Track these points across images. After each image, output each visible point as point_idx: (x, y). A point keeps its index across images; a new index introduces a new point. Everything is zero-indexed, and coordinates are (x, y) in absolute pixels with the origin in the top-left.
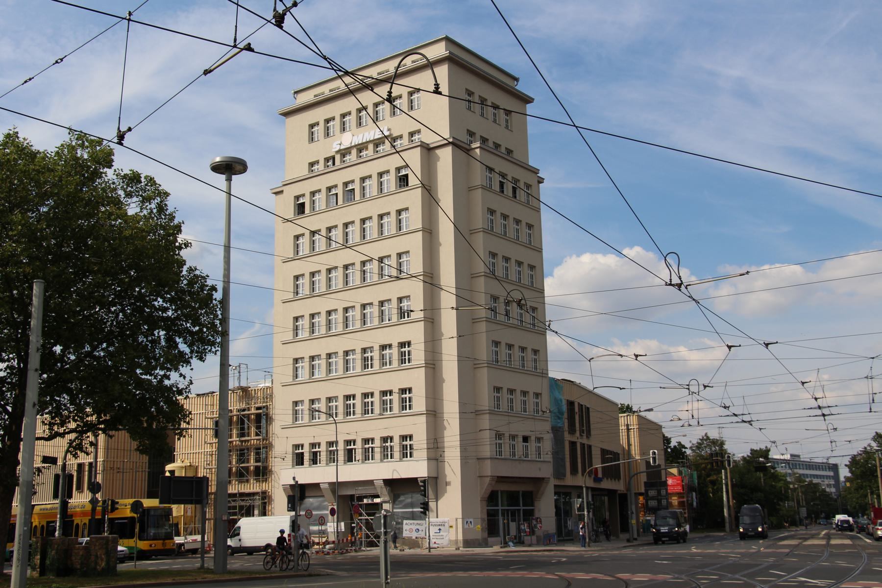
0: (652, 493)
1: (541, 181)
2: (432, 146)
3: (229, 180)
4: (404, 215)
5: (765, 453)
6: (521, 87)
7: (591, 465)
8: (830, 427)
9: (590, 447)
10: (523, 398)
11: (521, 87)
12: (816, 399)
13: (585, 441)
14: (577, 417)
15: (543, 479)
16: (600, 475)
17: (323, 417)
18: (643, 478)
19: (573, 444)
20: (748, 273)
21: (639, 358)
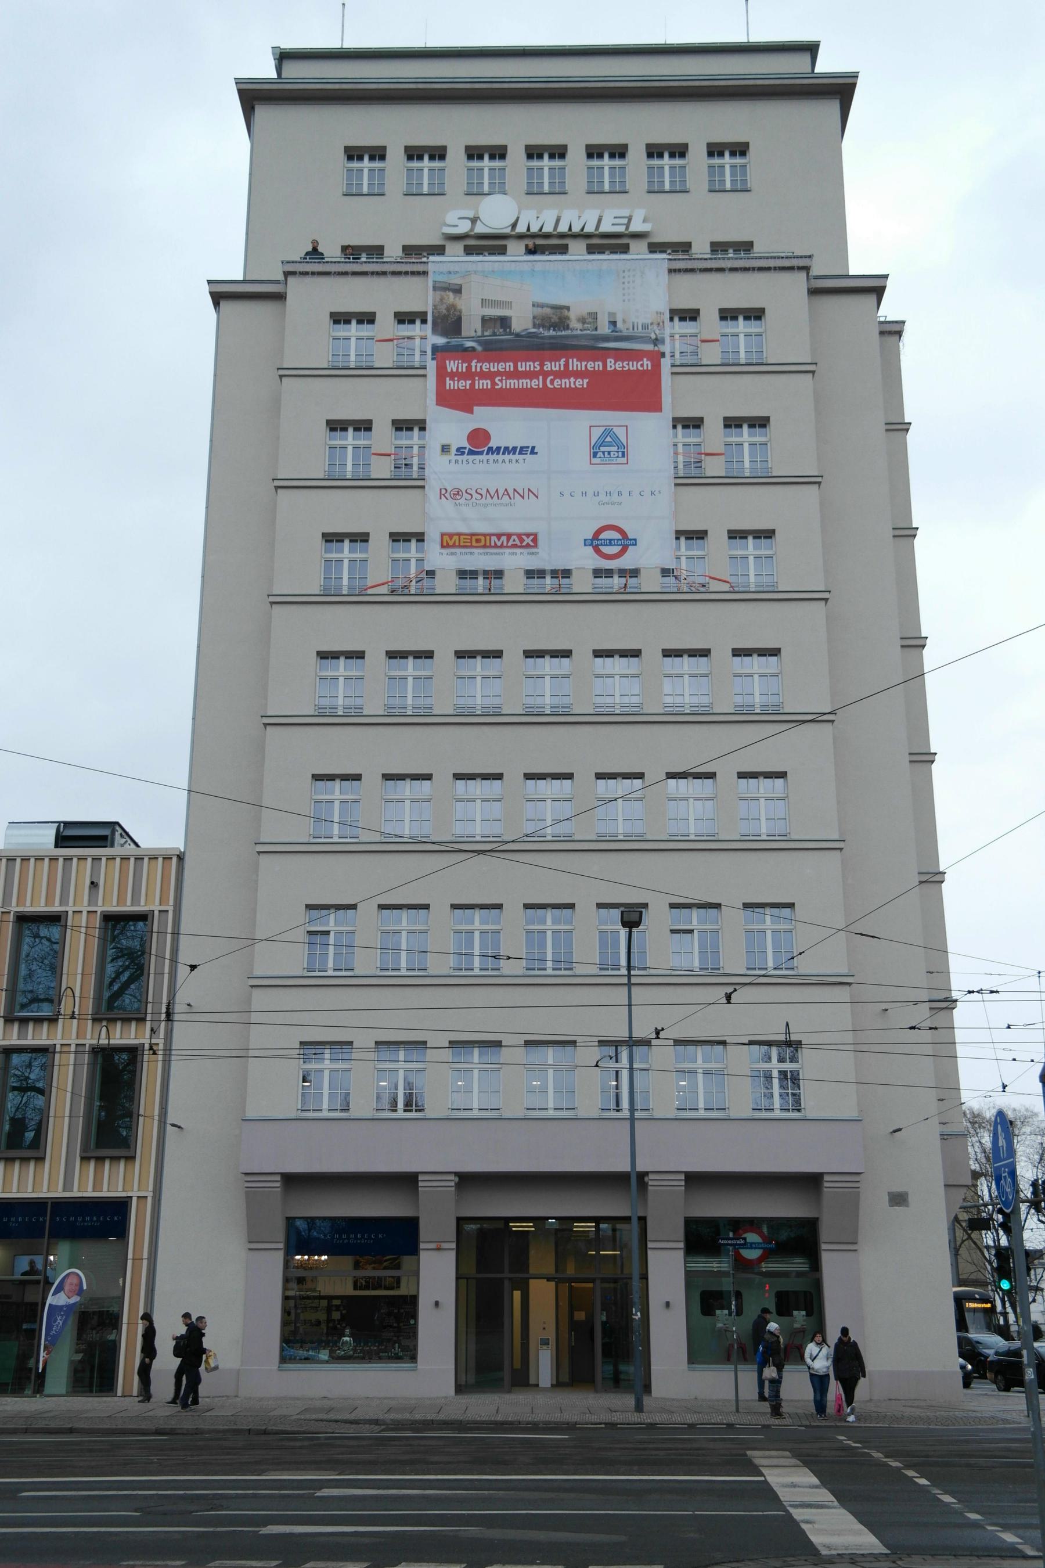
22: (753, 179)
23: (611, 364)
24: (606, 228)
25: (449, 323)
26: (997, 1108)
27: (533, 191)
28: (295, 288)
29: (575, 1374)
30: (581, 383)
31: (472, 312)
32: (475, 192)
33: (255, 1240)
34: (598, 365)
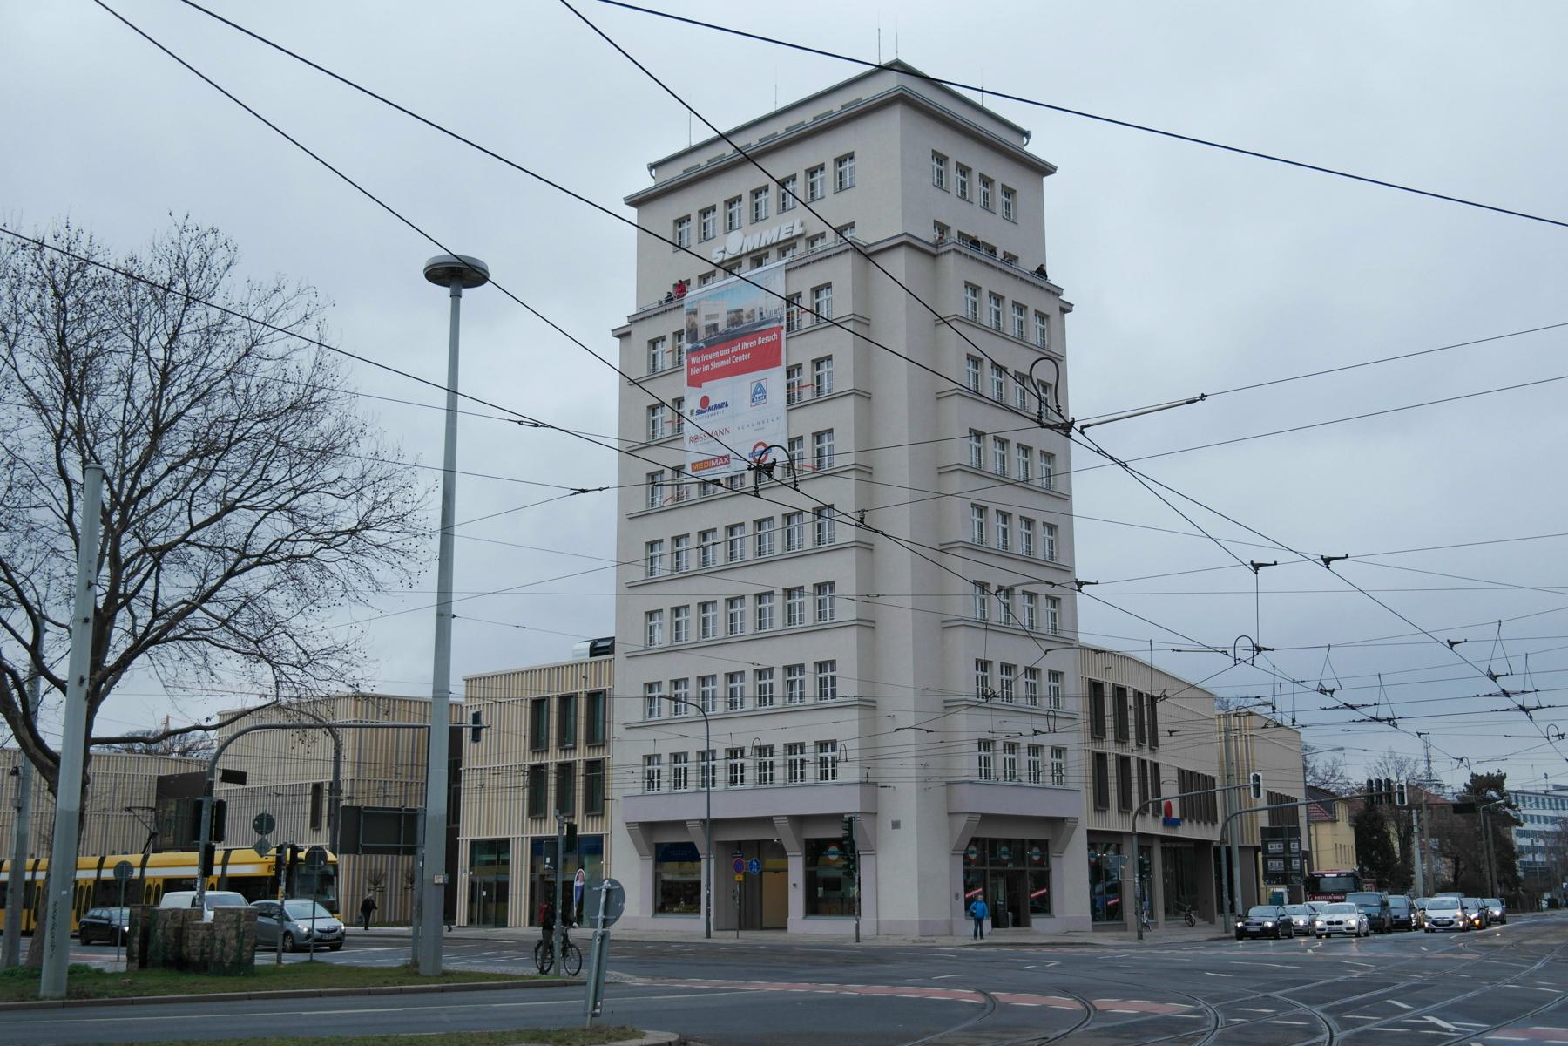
0: (1275, 847)
1: (1066, 308)
2: (871, 250)
3: (456, 296)
4: (825, 368)
5: (1496, 782)
6: (1034, 148)
7: (1157, 792)
8: (1553, 731)
9: (1156, 766)
10: (1053, 684)
11: (1033, 148)
12: (1494, 677)
13: (1146, 756)
14: (1131, 715)
15: (1063, 819)
16: (1176, 814)
17: (692, 711)
18: (1263, 820)
19: (1123, 762)
20: (1203, 397)
21: (1084, 588)
23: (761, 340)
24: (783, 237)
25: (693, 334)
28: (635, 330)
29: (813, 907)
30: (747, 356)
31: (702, 322)
34: (752, 344)
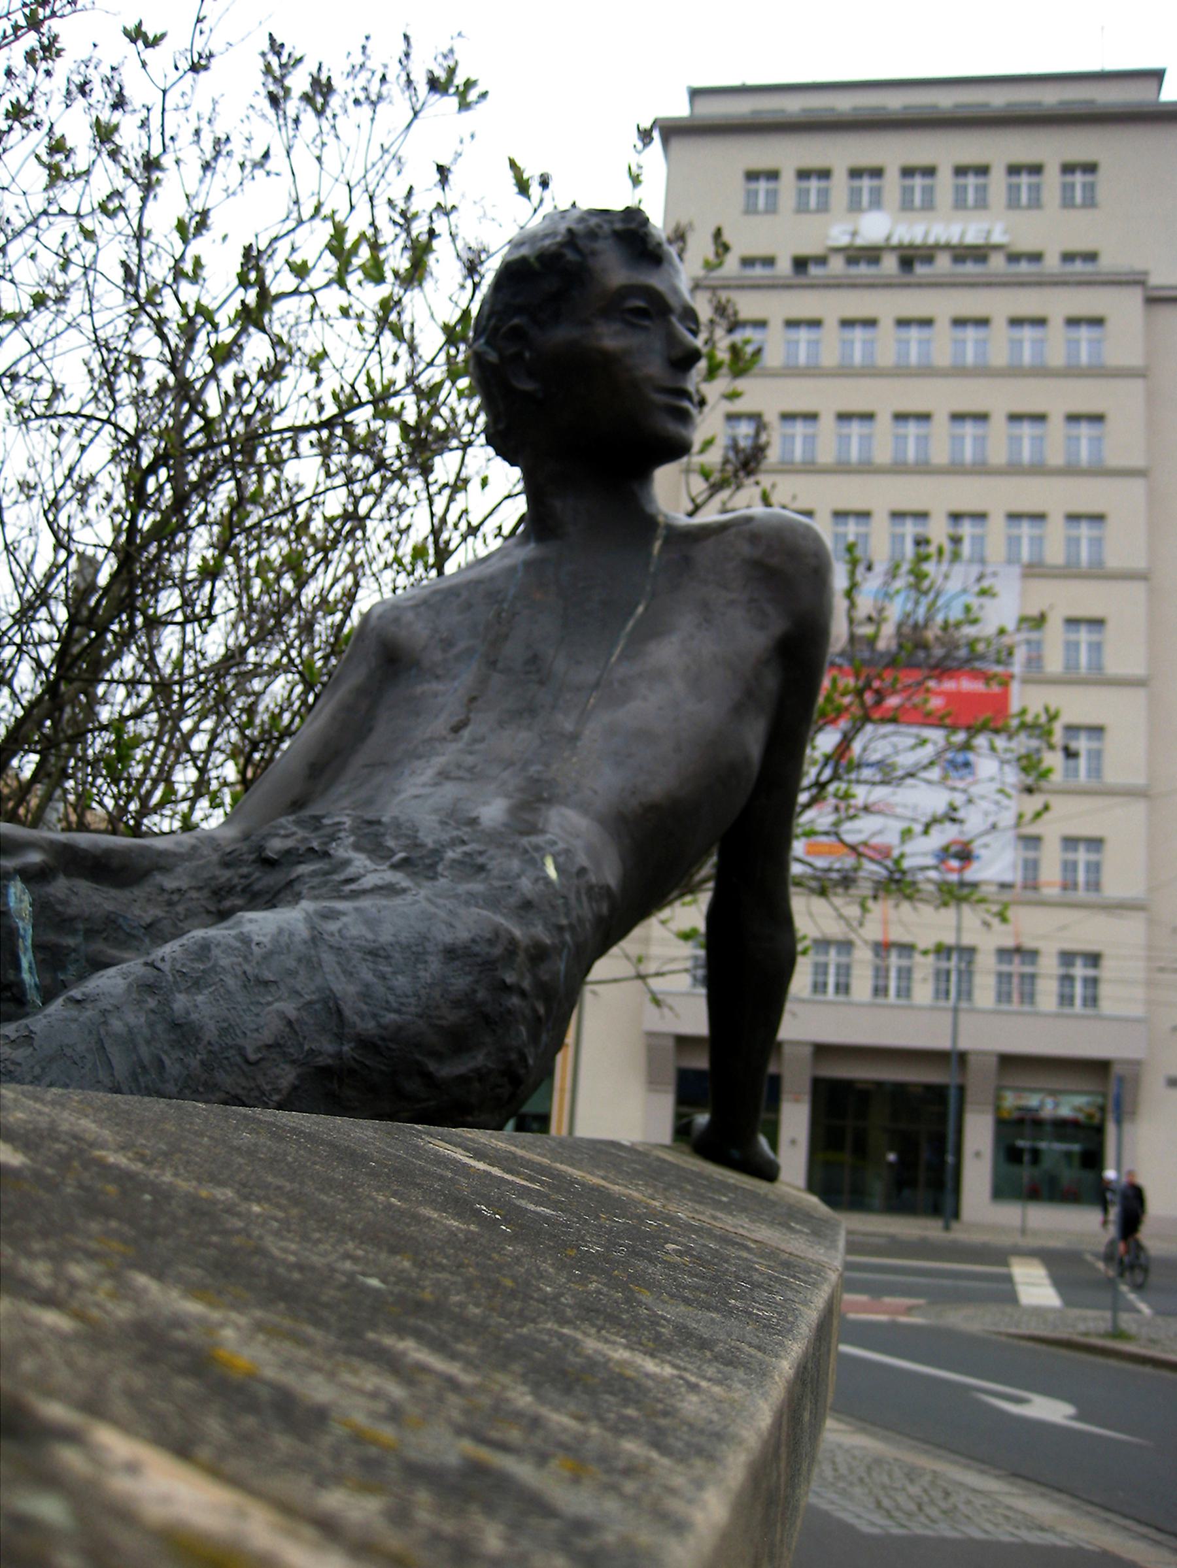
22: (1102, 193)
26: (496, 225)
27: (906, 205)
32: (855, 206)
33: (653, 1082)
